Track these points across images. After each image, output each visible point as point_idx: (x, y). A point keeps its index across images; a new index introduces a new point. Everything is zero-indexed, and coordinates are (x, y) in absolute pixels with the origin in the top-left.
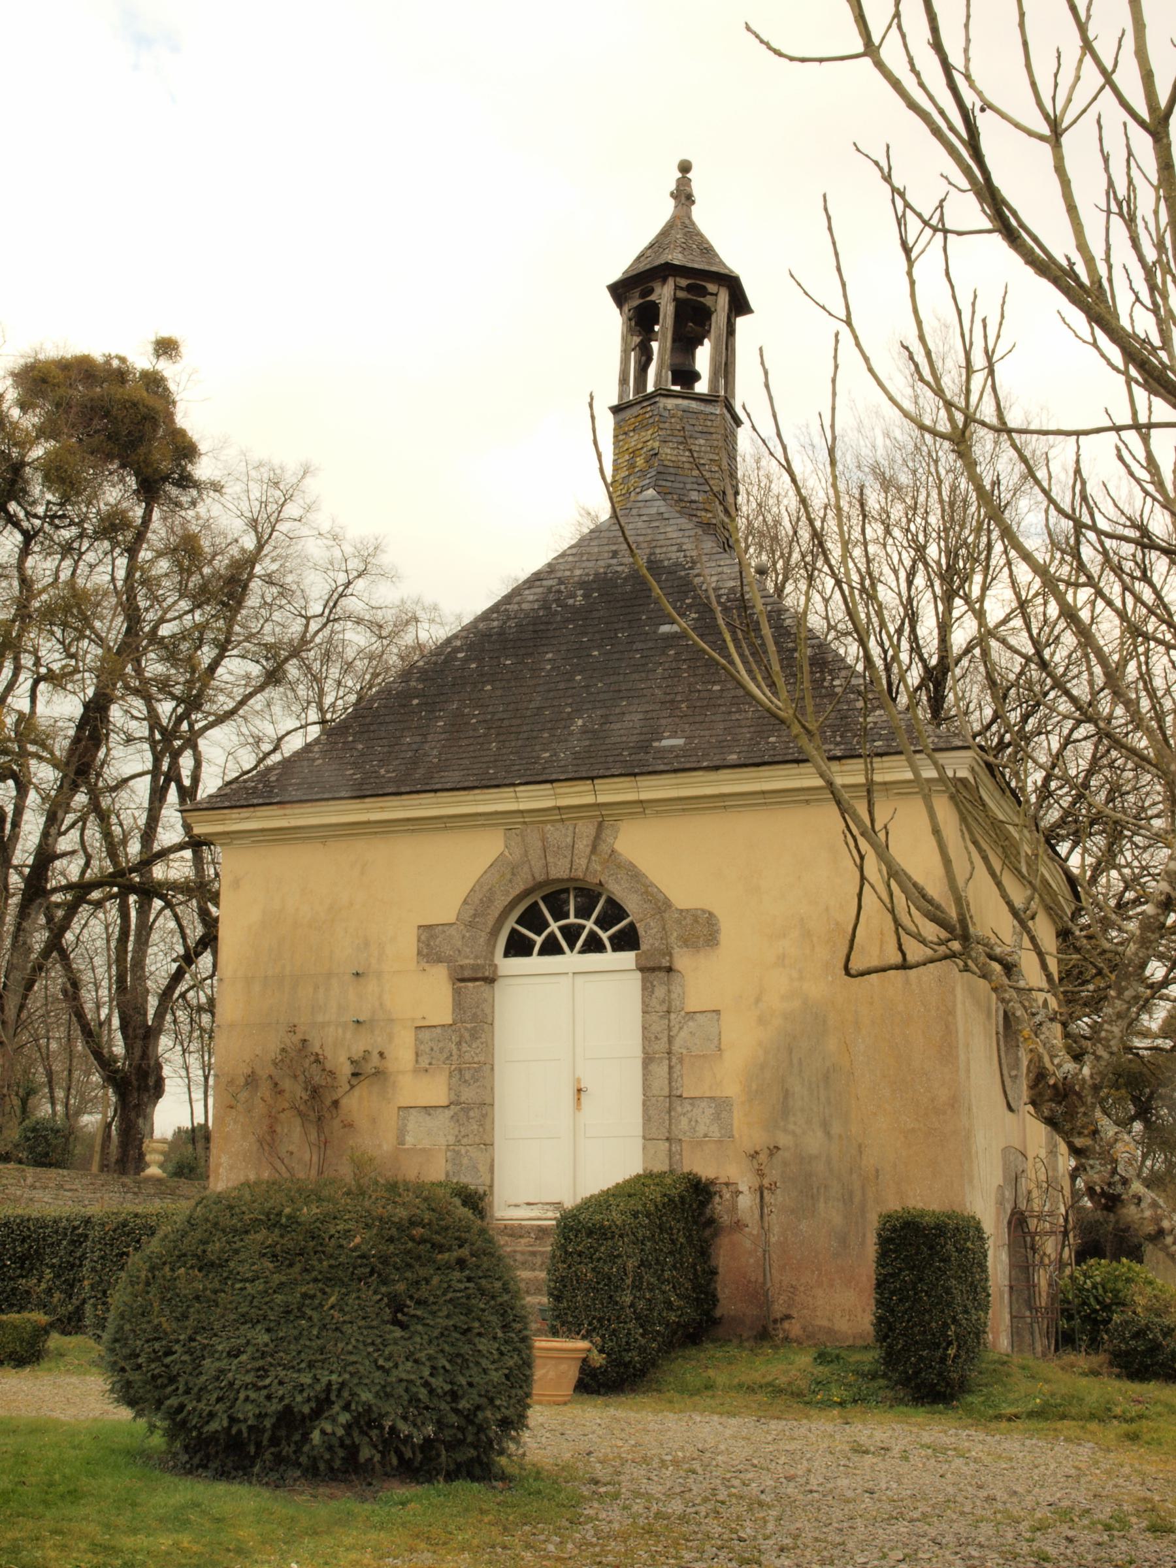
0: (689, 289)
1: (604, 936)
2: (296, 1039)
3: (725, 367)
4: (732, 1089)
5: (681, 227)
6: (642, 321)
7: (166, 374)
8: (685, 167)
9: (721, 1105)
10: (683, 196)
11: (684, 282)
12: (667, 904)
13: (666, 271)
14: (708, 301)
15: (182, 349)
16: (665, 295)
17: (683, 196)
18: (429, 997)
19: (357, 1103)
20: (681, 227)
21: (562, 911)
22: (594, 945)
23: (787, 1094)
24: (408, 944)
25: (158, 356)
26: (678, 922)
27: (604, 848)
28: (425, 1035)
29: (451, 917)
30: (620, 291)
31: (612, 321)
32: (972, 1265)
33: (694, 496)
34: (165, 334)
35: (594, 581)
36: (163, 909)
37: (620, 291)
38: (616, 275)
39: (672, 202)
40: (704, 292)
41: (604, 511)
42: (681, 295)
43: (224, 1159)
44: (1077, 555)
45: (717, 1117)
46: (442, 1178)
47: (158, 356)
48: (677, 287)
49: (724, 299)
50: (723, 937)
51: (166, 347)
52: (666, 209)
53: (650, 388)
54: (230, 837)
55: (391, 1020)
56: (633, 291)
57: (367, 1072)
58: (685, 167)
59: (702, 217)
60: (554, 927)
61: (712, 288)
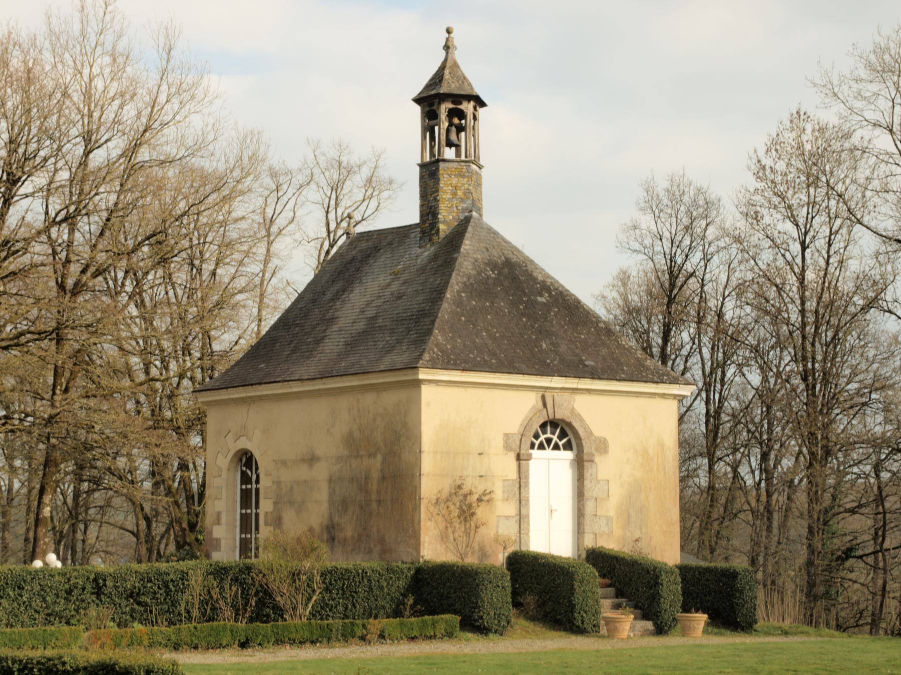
1: (561, 443)
4: (612, 513)
6: (430, 115)
9: (609, 519)
12: (591, 433)
18: (507, 466)
19: (481, 512)
21: (559, 431)
22: (556, 447)
23: (629, 516)
24: (499, 442)
26: (595, 441)
29: (516, 432)
43: (427, 539)
44: (833, 338)
45: (607, 524)
46: (422, 554)
50: (610, 451)
54: (430, 381)
55: (493, 476)
57: (485, 498)
60: (555, 438)
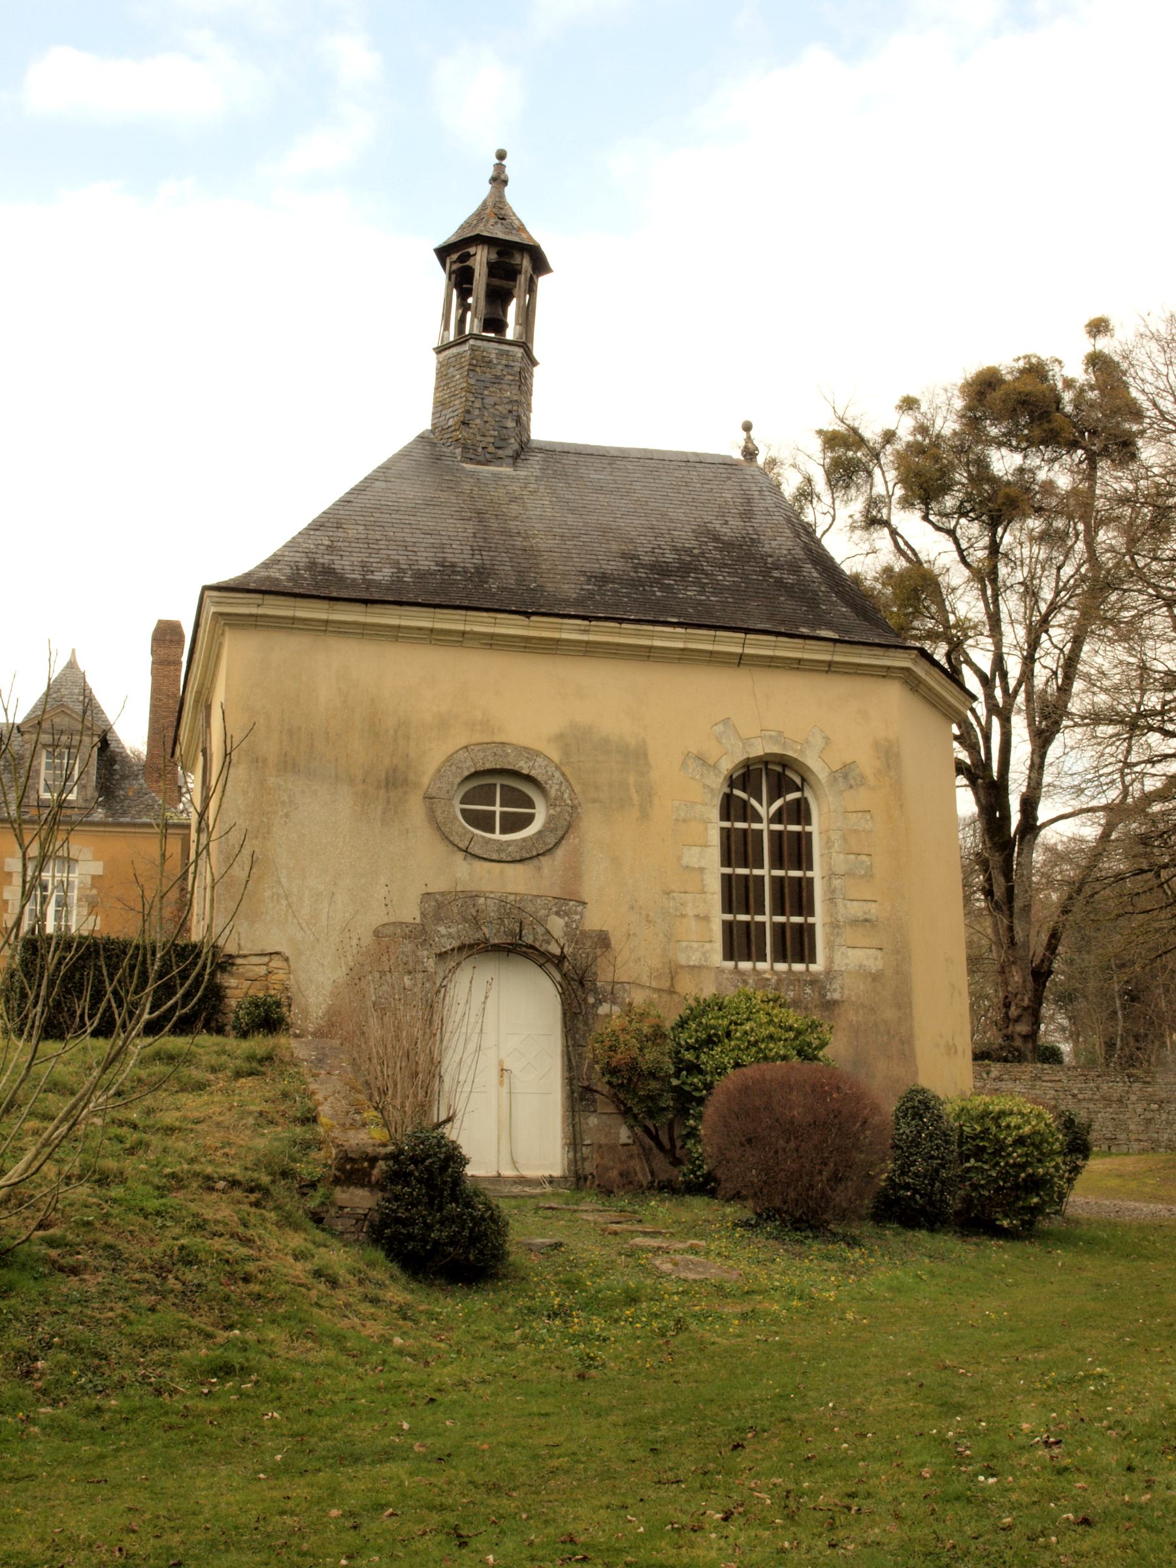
3: (527, 317)
5: (496, 209)
6: (461, 280)
8: (501, 155)
10: (499, 180)
11: (455, 257)
13: (478, 240)
16: (480, 259)
17: (499, 180)
20: (496, 209)
25: (1095, 337)
30: (443, 253)
31: (437, 278)
32: (791, 907)
35: (1076, 1042)
37: (443, 253)
38: (440, 241)
41: (430, 428)
42: (455, 267)
47: (1095, 337)
49: (526, 264)
51: (1098, 327)
52: (486, 189)
53: (467, 332)
56: (454, 254)
58: (501, 155)
61: (472, 250)
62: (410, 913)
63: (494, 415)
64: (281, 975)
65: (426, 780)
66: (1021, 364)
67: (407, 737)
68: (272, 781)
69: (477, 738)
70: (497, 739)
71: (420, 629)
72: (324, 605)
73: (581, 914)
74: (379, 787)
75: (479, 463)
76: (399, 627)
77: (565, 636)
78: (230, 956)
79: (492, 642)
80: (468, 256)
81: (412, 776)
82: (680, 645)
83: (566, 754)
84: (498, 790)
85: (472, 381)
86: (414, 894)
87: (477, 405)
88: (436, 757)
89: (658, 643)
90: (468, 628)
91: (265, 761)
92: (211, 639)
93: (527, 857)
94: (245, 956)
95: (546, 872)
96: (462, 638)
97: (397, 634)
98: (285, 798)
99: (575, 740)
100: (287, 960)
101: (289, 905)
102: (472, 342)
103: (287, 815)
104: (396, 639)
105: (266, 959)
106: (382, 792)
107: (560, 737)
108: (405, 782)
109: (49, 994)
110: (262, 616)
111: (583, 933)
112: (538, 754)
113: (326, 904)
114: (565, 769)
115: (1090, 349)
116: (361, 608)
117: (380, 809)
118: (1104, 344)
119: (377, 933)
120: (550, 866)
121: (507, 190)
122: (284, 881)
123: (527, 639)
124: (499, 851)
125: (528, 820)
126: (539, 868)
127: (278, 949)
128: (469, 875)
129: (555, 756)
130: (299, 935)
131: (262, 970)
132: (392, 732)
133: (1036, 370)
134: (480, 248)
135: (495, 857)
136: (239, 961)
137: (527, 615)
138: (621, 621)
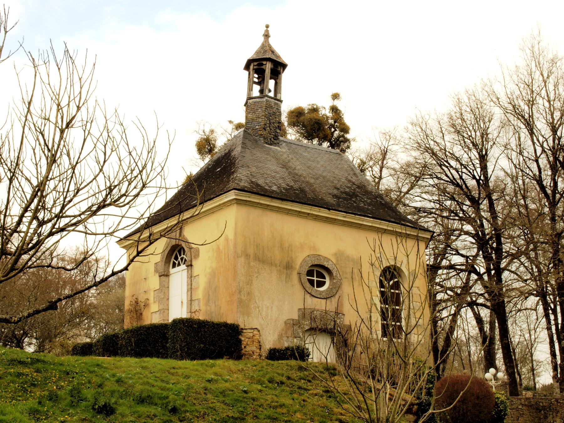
0: (257, 65)
2: (134, 298)
5: (266, 47)
7: (337, 106)
8: (267, 27)
11: (256, 63)
14: (263, 67)
15: (341, 96)
20: (266, 47)
27: (182, 235)
28: (156, 292)
33: (257, 127)
34: (335, 92)
36: (476, 280)
39: (263, 38)
40: (262, 64)
42: (255, 67)
48: (254, 66)
51: (335, 96)
52: (262, 39)
58: (267, 27)
59: (272, 41)
61: (264, 63)
62: (295, 316)
63: (273, 127)
64: (257, 337)
65: (298, 267)
66: (310, 107)
67: (292, 251)
68: (252, 264)
69: (312, 253)
70: (317, 254)
71: (296, 211)
72: (269, 199)
73: (343, 319)
74: (284, 268)
75: (269, 144)
76: (290, 210)
77: (339, 218)
78: (242, 329)
79: (317, 218)
80: (262, 64)
81: (293, 265)
82: (370, 224)
83: (337, 261)
84: (317, 273)
85: (267, 113)
86: (296, 310)
87: (268, 122)
88: (301, 259)
89: (365, 223)
90: (311, 212)
91: (250, 256)
92: (408, 222)
93: (327, 297)
94: (246, 329)
95: (333, 303)
96: (307, 216)
97: (288, 212)
98: (256, 270)
99: (339, 255)
100: (259, 331)
101: (259, 311)
102: (266, 98)
103: (257, 277)
104: (288, 214)
105: (252, 331)
106: (285, 270)
107: (335, 254)
108: (292, 267)
109: (556, 319)
110: (249, 201)
111: (344, 325)
112: (329, 260)
113: (270, 311)
114: (337, 266)
115: (331, 104)
116: (280, 202)
117: (285, 277)
118: (337, 103)
119: (285, 322)
120: (334, 300)
121: (270, 39)
122: (257, 301)
123: (327, 218)
124: (320, 294)
125: (323, 284)
126: (331, 302)
127: (256, 327)
128: (312, 303)
129: (334, 261)
130: (263, 322)
131: (251, 335)
132: (287, 249)
133: (315, 110)
134: (268, 63)
135: (319, 296)
136: (244, 331)
137: (329, 209)
138: (355, 214)
